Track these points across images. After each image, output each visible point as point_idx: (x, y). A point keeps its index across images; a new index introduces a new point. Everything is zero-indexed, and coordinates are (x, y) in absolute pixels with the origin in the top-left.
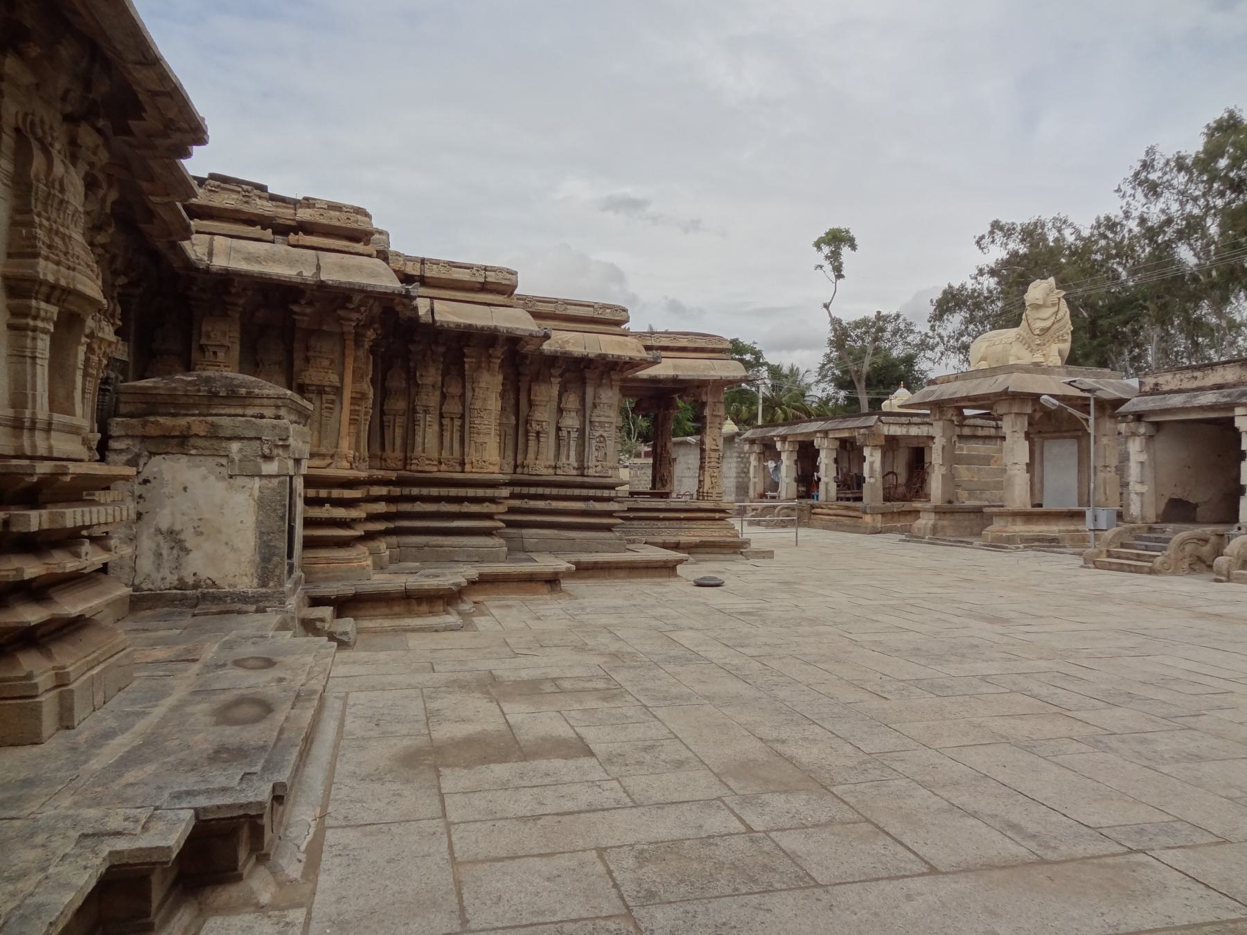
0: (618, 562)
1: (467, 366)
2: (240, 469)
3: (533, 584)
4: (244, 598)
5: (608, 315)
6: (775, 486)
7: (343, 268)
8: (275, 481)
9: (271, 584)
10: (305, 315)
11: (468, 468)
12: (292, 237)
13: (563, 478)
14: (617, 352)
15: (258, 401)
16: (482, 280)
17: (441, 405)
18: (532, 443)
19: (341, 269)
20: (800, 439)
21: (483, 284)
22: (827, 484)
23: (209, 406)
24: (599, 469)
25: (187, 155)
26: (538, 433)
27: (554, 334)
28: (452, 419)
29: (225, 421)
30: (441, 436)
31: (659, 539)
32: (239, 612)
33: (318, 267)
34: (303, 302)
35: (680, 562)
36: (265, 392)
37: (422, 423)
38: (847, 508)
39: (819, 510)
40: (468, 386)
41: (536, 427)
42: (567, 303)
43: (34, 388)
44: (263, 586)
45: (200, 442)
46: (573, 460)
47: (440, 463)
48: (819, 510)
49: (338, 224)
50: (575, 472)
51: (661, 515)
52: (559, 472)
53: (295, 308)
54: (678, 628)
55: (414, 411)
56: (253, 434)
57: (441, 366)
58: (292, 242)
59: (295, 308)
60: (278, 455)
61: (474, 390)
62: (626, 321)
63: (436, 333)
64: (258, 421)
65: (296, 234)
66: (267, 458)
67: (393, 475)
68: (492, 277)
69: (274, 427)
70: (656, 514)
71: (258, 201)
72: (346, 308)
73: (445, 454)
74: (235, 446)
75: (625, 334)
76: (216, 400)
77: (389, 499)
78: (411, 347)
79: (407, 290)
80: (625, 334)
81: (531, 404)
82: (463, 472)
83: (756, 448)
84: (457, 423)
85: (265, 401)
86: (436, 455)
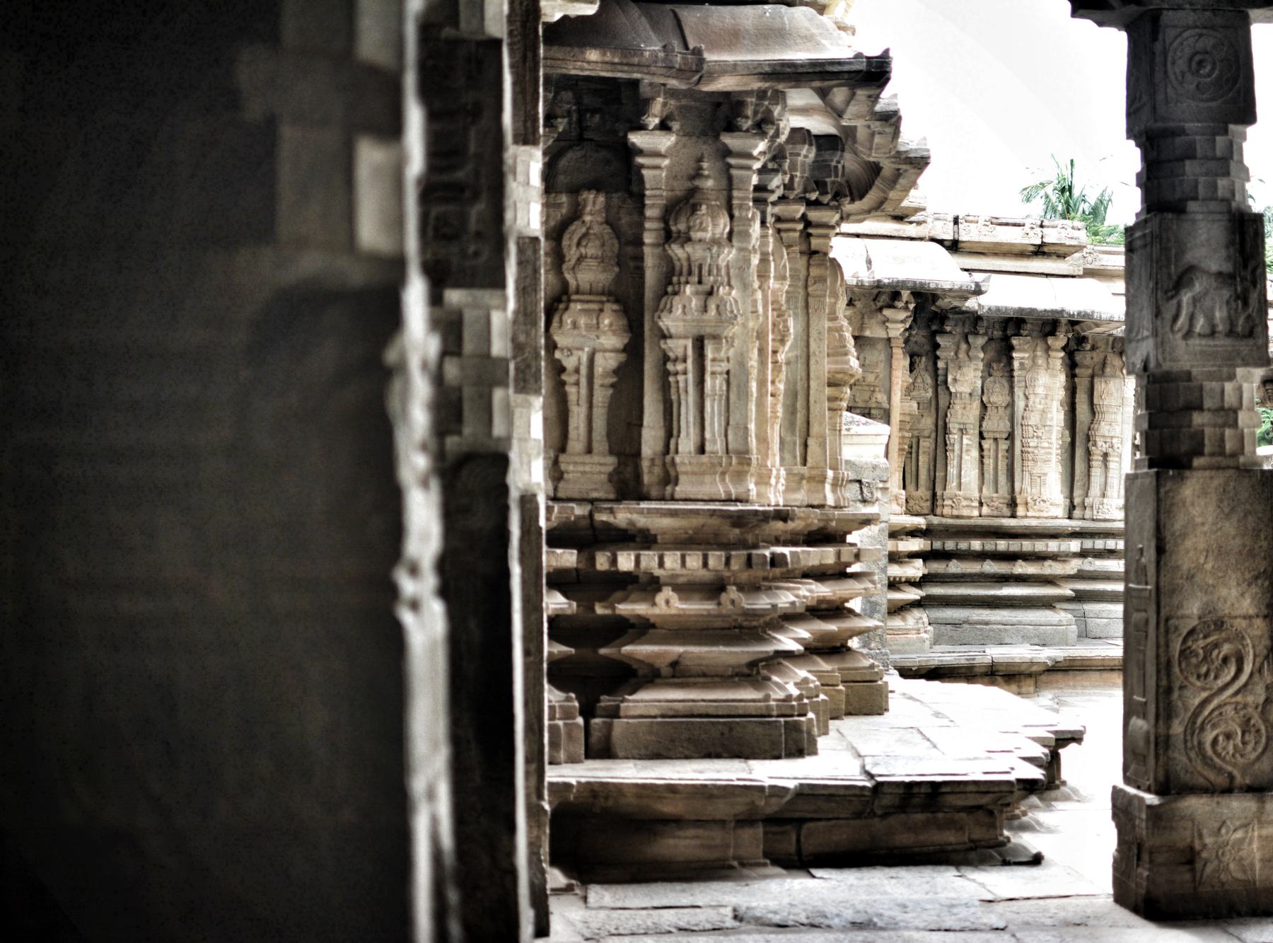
1: (1016, 364)
9: (873, 645)
11: (1020, 511)
16: (1039, 242)
17: (982, 419)
18: (1097, 472)
21: (1040, 246)
26: (1106, 455)
28: (996, 439)
30: (982, 463)
37: (957, 447)
40: (1019, 392)
41: (1101, 446)
47: (981, 504)
53: (636, 139)
57: (981, 365)
59: (636, 139)
67: (920, 522)
72: (894, 307)
73: (986, 492)
77: (925, 556)
78: (939, 339)
82: (1013, 516)
84: (1004, 446)
86: (977, 495)
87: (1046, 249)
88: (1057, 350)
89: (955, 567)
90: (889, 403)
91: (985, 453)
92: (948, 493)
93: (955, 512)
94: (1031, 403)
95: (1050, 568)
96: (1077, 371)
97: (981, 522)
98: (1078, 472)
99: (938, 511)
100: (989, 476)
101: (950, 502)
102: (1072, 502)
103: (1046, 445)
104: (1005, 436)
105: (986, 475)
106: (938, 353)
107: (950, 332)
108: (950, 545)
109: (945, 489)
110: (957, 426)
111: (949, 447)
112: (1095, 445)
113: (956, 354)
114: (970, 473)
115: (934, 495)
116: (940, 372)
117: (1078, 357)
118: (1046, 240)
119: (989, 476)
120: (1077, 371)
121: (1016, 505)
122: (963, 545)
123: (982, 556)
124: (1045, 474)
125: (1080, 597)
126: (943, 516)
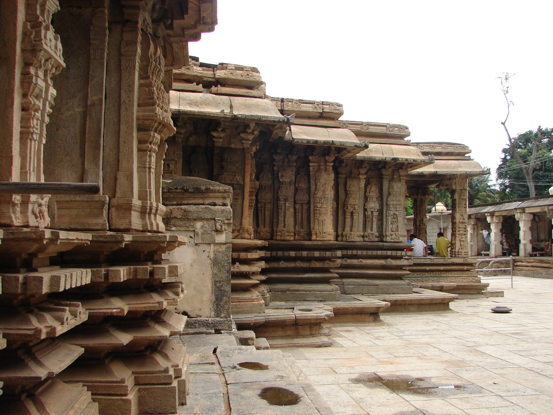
0: (411, 300)
1: (311, 168)
2: (202, 240)
3: (363, 316)
4: (206, 324)
5: (396, 131)
6: (487, 247)
7: (248, 107)
8: (224, 247)
9: (223, 315)
10: (220, 138)
11: (314, 237)
12: (214, 89)
13: (369, 244)
14: (405, 157)
15: (211, 195)
16: (321, 111)
17: (295, 194)
18: (348, 220)
19: (243, 107)
20: (504, 214)
21: (321, 113)
22: (525, 245)
23: (183, 199)
24: (394, 236)
25: (196, 37)
26: (352, 213)
27: (371, 146)
28: (302, 204)
29: (192, 208)
31: (430, 284)
32: (207, 334)
33: (231, 107)
34: (220, 130)
35: (452, 299)
36: (217, 188)
37: (283, 207)
38: (541, 261)
39: (520, 263)
40: (312, 182)
41: (350, 209)
42: (369, 124)
43: (150, 188)
44: (217, 317)
45: (178, 223)
46: (375, 231)
47: (295, 234)
48: (520, 263)
49: (242, 78)
50: (376, 239)
51: (428, 268)
52: (366, 239)
53: (215, 134)
54: (480, 345)
55: (278, 200)
56: (209, 216)
57: (295, 169)
58: (213, 91)
59: (215, 134)
60: (225, 230)
61: (316, 185)
62: (409, 135)
63: (292, 146)
64: (213, 207)
65: (216, 86)
66: (218, 231)
68: (327, 109)
69: (223, 211)
70: (424, 268)
71: (195, 68)
72: (247, 133)
74: (199, 225)
75: (407, 144)
76: (187, 195)
78: (275, 157)
79: (288, 119)
80: (407, 144)
81: (347, 194)
83: (472, 222)
84: (305, 207)
85: (217, 194)
86: (293, 230)
87: (325, 115)
88: (330, 162)
89: (283, 264)
90: (244, 181)
91: (297, 210)
92: (279, 229)
93: (282, 238)
94: (318, 187)
95: (327, 264)
96: (339, 176)
97: (295, 242)
98: (340, 220)
99: (275, 238)
100: (299, 221)
101: (280, 234)
102: (337, 234)
103: (325, 206)
104: (306, 202)
105: (297, 221)
106: (274, 163)
107: (280, 153)
108: (280, 253)
109: (278, 227)
110: (283, 197)
111: (279, 208)
112: (347, 208)
113: (283, 164)
114: (290, 221)
115: (273, 230)
116: (275, 172)
117: (340, 170)
118: (325, 110)
119: (299, 221)
120: (339, 176)
121: (311, 235)
122: (286, 254)
123: (294, 259)
124: (325, 220)
125: (342, 276)
126: (276, 240)
